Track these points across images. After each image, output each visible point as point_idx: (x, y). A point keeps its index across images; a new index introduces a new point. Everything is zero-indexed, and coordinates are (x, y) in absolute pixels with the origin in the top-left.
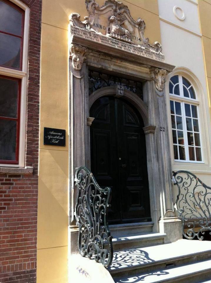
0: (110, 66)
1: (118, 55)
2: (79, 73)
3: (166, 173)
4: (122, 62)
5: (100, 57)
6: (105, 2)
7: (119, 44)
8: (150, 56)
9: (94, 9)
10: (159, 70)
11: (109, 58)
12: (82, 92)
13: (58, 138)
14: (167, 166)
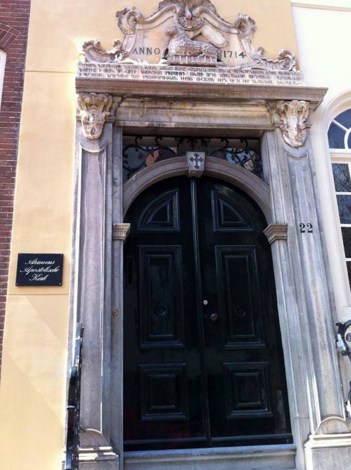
0: (170, 118)
1: (180, 94)
2: (98, 144)
3: (321, 328)
4: (194, 105)
5: (146, 106)
6: (158, 5)
7: (185, 72)
8: (262, 80)
9: (135, 22)
10: (286, 103)
11: (165, 105)
12: (102, 179)
13: (46, 270)
14: (322, 312)
